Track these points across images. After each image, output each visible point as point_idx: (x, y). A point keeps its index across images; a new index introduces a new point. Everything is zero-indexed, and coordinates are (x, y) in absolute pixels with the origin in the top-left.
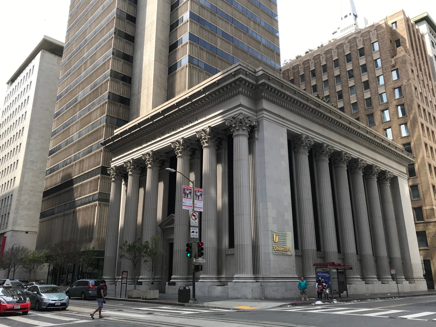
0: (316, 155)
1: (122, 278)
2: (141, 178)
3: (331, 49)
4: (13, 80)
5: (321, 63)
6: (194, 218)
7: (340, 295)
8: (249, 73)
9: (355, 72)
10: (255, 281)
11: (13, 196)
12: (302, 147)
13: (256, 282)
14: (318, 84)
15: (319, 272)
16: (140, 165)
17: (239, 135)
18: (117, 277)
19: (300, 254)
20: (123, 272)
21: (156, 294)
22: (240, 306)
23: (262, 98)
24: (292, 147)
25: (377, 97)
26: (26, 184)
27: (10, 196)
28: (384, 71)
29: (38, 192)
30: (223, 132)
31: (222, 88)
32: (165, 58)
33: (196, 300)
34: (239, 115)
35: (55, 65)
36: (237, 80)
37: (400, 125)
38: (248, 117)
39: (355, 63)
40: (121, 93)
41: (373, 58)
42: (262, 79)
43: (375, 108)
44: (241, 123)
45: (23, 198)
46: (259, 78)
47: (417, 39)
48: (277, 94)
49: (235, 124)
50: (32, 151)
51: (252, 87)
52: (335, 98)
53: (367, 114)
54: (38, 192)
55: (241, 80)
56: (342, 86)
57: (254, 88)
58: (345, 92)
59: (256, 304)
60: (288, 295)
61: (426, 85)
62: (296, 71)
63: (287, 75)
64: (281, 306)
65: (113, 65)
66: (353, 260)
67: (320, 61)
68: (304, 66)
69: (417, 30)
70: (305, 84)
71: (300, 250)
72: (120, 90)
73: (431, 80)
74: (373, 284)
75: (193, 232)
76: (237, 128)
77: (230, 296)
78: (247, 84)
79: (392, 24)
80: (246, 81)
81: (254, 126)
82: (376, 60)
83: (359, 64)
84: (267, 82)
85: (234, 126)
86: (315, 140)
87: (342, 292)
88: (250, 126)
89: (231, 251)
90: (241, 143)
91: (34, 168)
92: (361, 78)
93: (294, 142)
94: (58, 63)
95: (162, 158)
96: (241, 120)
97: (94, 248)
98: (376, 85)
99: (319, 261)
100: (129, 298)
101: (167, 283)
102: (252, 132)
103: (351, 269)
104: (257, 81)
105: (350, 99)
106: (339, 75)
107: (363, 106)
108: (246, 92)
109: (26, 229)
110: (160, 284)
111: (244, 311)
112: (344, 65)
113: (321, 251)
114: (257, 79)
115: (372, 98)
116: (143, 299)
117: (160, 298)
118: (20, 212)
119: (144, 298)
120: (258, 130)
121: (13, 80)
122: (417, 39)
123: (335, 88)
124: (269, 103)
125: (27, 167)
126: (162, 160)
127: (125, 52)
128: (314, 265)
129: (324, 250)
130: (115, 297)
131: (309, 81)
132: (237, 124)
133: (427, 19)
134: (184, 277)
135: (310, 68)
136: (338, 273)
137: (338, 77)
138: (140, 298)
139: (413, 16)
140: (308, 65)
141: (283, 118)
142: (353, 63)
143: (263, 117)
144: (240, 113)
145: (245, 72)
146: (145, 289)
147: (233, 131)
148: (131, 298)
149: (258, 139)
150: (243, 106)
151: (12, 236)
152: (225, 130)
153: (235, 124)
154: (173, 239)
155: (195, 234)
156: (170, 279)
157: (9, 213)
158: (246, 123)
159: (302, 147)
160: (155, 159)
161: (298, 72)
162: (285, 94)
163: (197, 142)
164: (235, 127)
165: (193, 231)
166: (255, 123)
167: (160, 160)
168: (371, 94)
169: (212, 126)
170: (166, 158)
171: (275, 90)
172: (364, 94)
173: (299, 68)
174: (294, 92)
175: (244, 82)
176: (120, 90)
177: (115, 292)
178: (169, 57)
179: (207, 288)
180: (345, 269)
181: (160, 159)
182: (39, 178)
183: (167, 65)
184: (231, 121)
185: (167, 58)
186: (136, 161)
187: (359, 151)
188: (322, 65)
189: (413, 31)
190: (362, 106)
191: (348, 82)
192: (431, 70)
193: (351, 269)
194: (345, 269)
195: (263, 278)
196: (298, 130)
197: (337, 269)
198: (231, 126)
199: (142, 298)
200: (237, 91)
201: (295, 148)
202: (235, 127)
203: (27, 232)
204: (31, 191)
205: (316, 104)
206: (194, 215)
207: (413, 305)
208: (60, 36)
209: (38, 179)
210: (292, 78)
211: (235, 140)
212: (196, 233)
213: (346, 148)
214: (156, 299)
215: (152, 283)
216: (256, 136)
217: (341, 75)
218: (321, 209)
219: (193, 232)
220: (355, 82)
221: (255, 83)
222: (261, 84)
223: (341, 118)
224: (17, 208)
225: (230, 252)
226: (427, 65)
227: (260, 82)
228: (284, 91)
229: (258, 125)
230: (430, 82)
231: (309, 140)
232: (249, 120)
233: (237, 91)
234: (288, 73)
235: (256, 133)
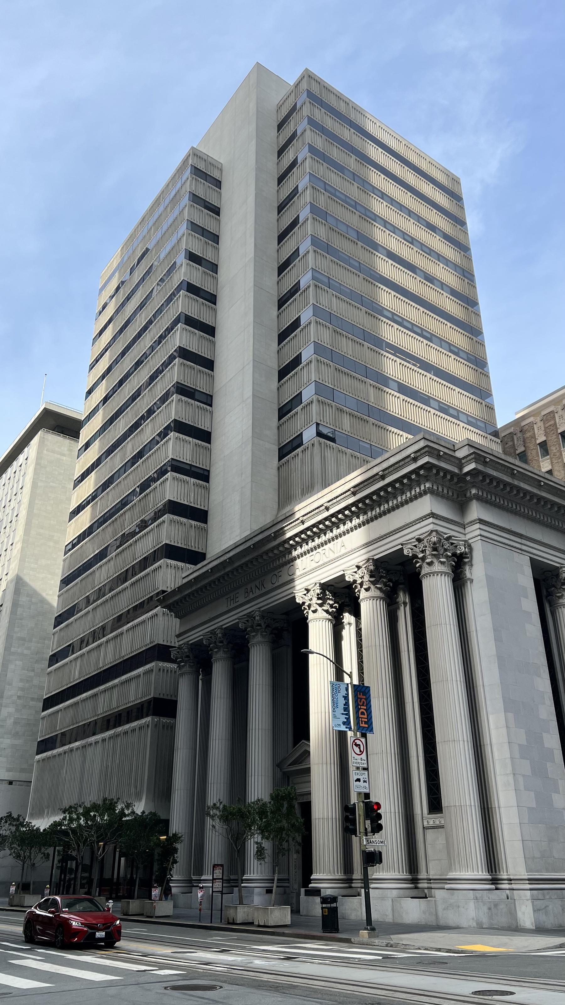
1: (213, 879)
6: (357, 750)
8: (445, 453)
13: (497, 889)
17: (433, 573)
18: (194, 878)
20: (215, 866)
21: (281, 915)
24: (544, 593)
26: (10, 684)
29: (33, 699)
30: (399, 568)
33: (373, 929)
35: (64, 455)
40: (192, 500)
42: (469, 462)
44: (435, 549)
46: (463, 461)
49: (422, 552)
50: (21, 619)
51: (452, 479)
54: (33, 699)
57: (456, 480)
59: (504, 939)
63: (510, 443)
70: (551, 459)
75: (358, 780)
76: (428, 561)
81: (461, 554)
84: (481, 467)
85: (421, 555)
88: (454, 555)
90: (437, 589)
91: (26, 652)
96: (435, 543)
97: (143, 812)
101: (303, 890)
102: (458, 565)
104: (461, 468)
108: (440, 489)
110: (285, 893)
111: (483, 956)
114: (460, 463)
116: (259, 926)
119: (262, 923)
120: (471, 561)
125: (13, 649)
131: (558, 454)
132: (428, 552)
134: (337, 877)
135: (557, 429)
138: (252, 924)
141: (521, 536)
144: (432, 531)
146: (257, 904)
147: (420, 567)
149: (472, 581)
150: (438, 515)
152: (402, 564)
154: (310, 794)
155: (361, 783)
156: (310, 881)
158: (446, 550)
161: (534, 437)
162: (519, 489)
163: (346, 590)
164: (423, 559)
169: (376, 557)
173: (533, 429)
175: (434, 471)
177: (200, 910)
179: (391, 903)
182: (33, 671)
183: (277, 444)
184: (415, 546)
195: (511, 880)
201: (549, 594)
202: (423, 559)
203: (11, 783)
204: (19, 697)
205: (409, 363)
206: (357, 745)
208: (75, 406)
209: (32, 674)
210: (521, 449)
211: (426, 583)
212: (365, 781)
219: (358, 780)
225: (431, 823)
227: (466, 469)
228: (516, 482)
232: (452, 544)
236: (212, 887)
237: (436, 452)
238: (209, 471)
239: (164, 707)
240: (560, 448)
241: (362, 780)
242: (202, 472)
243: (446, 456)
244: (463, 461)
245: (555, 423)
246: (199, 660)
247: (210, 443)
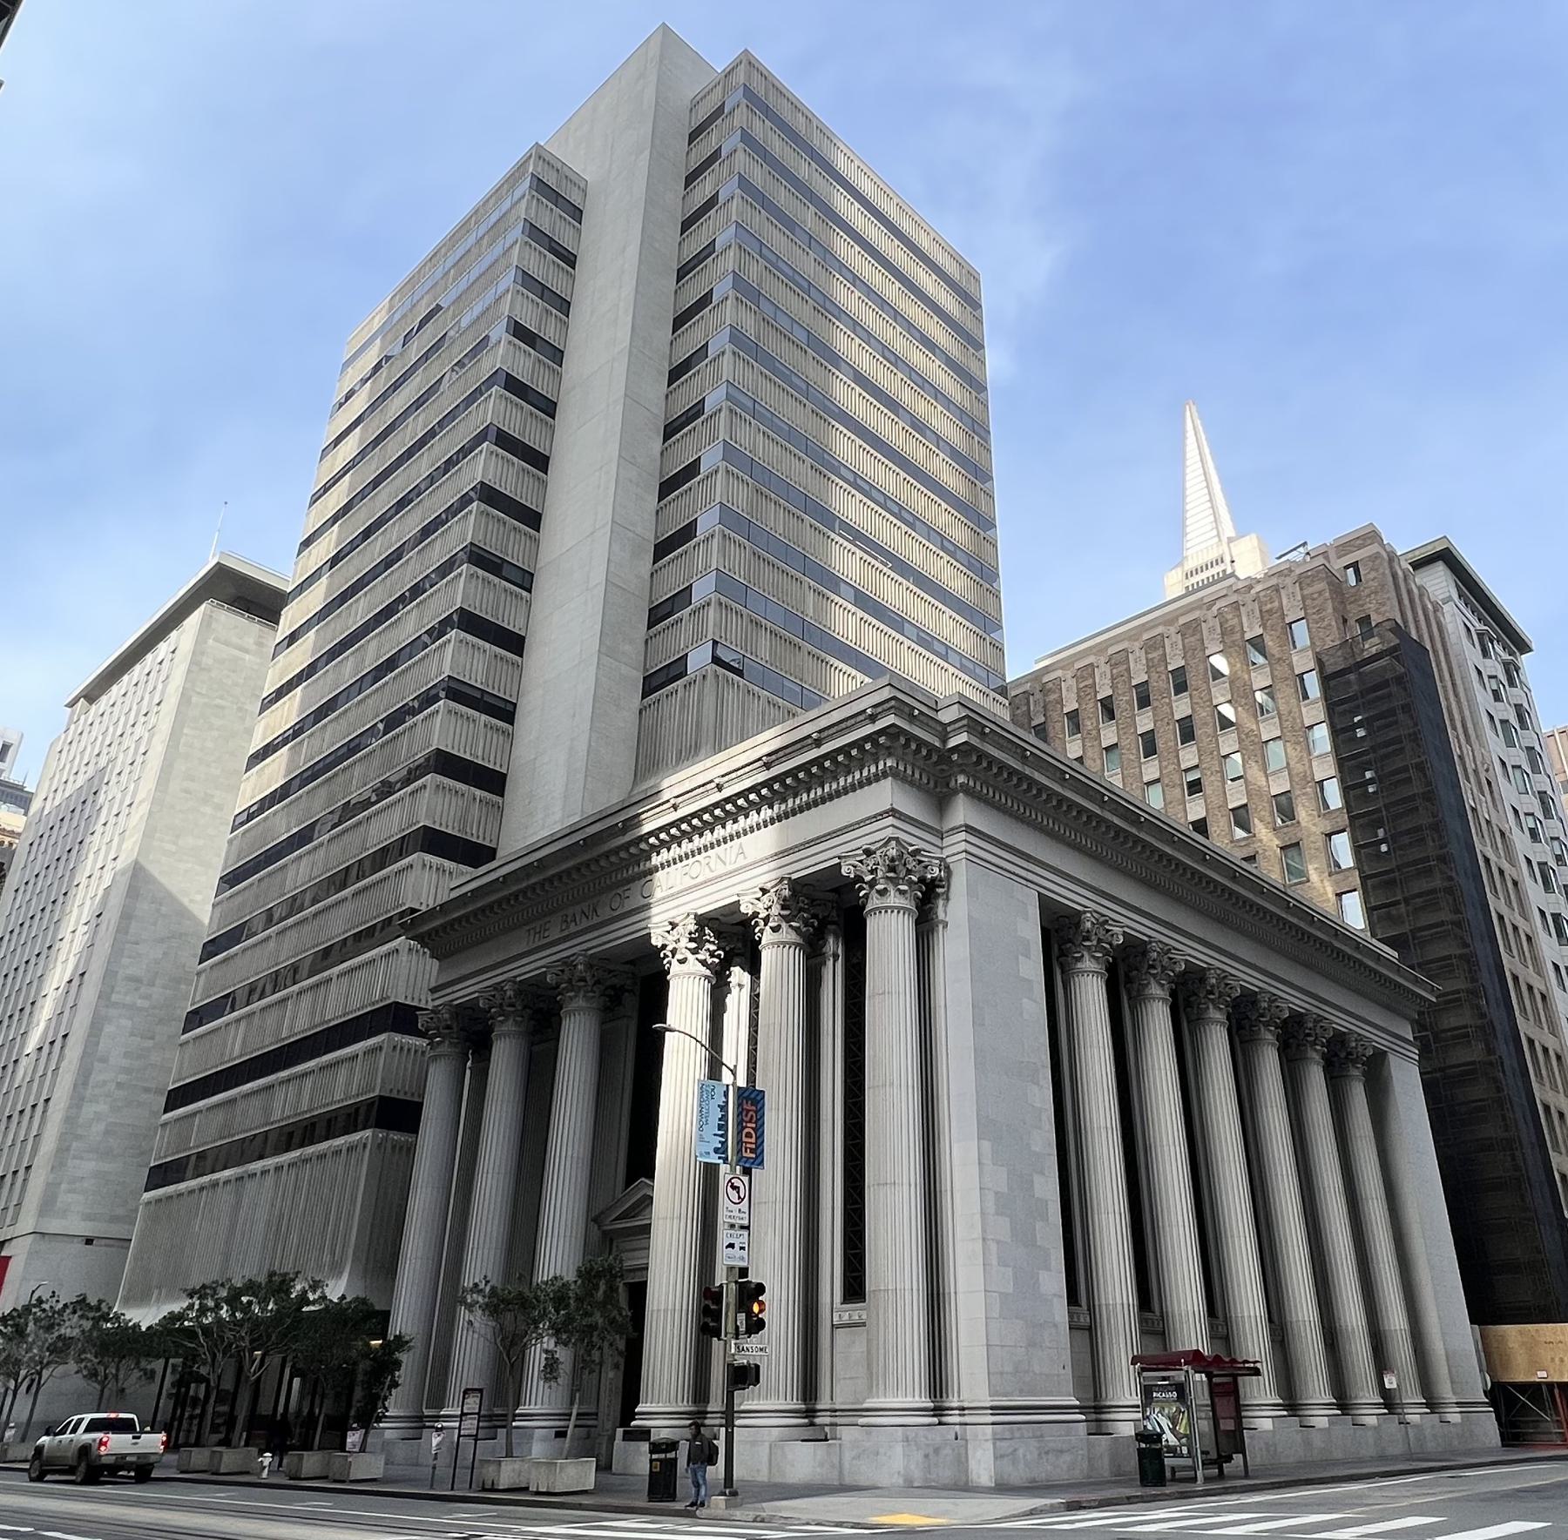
0: (1129, 980)
1: (463, 1414)
2: (536, 1048)
3: (1161, 635)
4: (92, 694)
6: (733, 1195)
10: (936, 1420)
11: (51, 1103)
12: (1087, 956)
13: (940, 1424)
15: (187, 1437)
19: (1084, 1320)
21: (581, 1474)
22: (882, 1513)
26: (104, 1060)
27: (29, 1109)
29: (147, 1090)
33: (734, 1494)
34: (885, 845)
35: (247, 651)
37: (1329, 835)
41: (1292, 669)
42: (958, 731)
44: (892, 869)
45: (88, 1110)
47: (1406, 602)
48: (1017, 785)
49: (872, 872)
54: (147, 1090)
57: (935, 758)
59: (945, 1504)
60: (1044, 1470)
61: (1470, 771)
64: (1032, 1513)
66: (1254, 1343)
67: (1128, 670)
69: (1419, 588)
70: (1083, 740)
71: (1085, 1307)
73: (1468, 741)
75: (731, 1246)
76: (879, 887)
77: (848, 1480)
78: (924, 752)
79: (1347, 567)
80: (910, 738)
81: (933, 879)
82: (1301, 676)
85: (868, 878)
87: (1229, 1459)
88: (922, 880)
89: (853, 1312)
93: (1061, 935)
94: (260, 644)
95: (615, 981)
96: (893, 860)
99: (1154, 1349)
100: (484, 1490)
101: (620, 1431)
102: (927, 899)
103: (1257, 1372)
108: (909, 772)
109: (86, 1229)
110: (588, 1437)
112: (1204, 687)
114: (944, 731)
117: (599, 1489)
118: (70, 1163)
121: (92, 694)
122: (1406, 602)
124: (1008, 820)
125: (114, 998)
126: (613, 987)
128: (1134, 1361)
130: (432, 1487)
132: (880, 874)
133: (1446, 557)
136: (1214, 1390)
139: (1405, 541)
140: (1090, 681)
145: (907, 709)
148: (493, 1490)
149: (946, 925)
151: (32, 1254)
152: (836, 890)
153: (872, 872)
157: (28, 1168)
158: (909, 872)
164: (872, 884)
169: (794, 876)
171: (1003, 766)
180: (1235, 1377)
182: (152, 1038)
188: (1134, 683)
189: (1409, 592)
192: (1467, 713)
193: (1257, 1372)
196: (1071, 897)
197: (1210, 1376)
198: (859, 879)
199: (533, 1488)
202: (872, 884)
203: (89, 1241)
204: (119, 1085)
206: (733, 1187)
207: (1467, 1499)
214: (585, 1492)
215: (561, 1434)
216: (941, 915)
219: (731, 1246)
224: (62, 1150)
225: (846, 1317)
226: (1456, 695)
227: (952, 743)
228: (1028, 771)
230: (1466, 749)
232: (920, 862)
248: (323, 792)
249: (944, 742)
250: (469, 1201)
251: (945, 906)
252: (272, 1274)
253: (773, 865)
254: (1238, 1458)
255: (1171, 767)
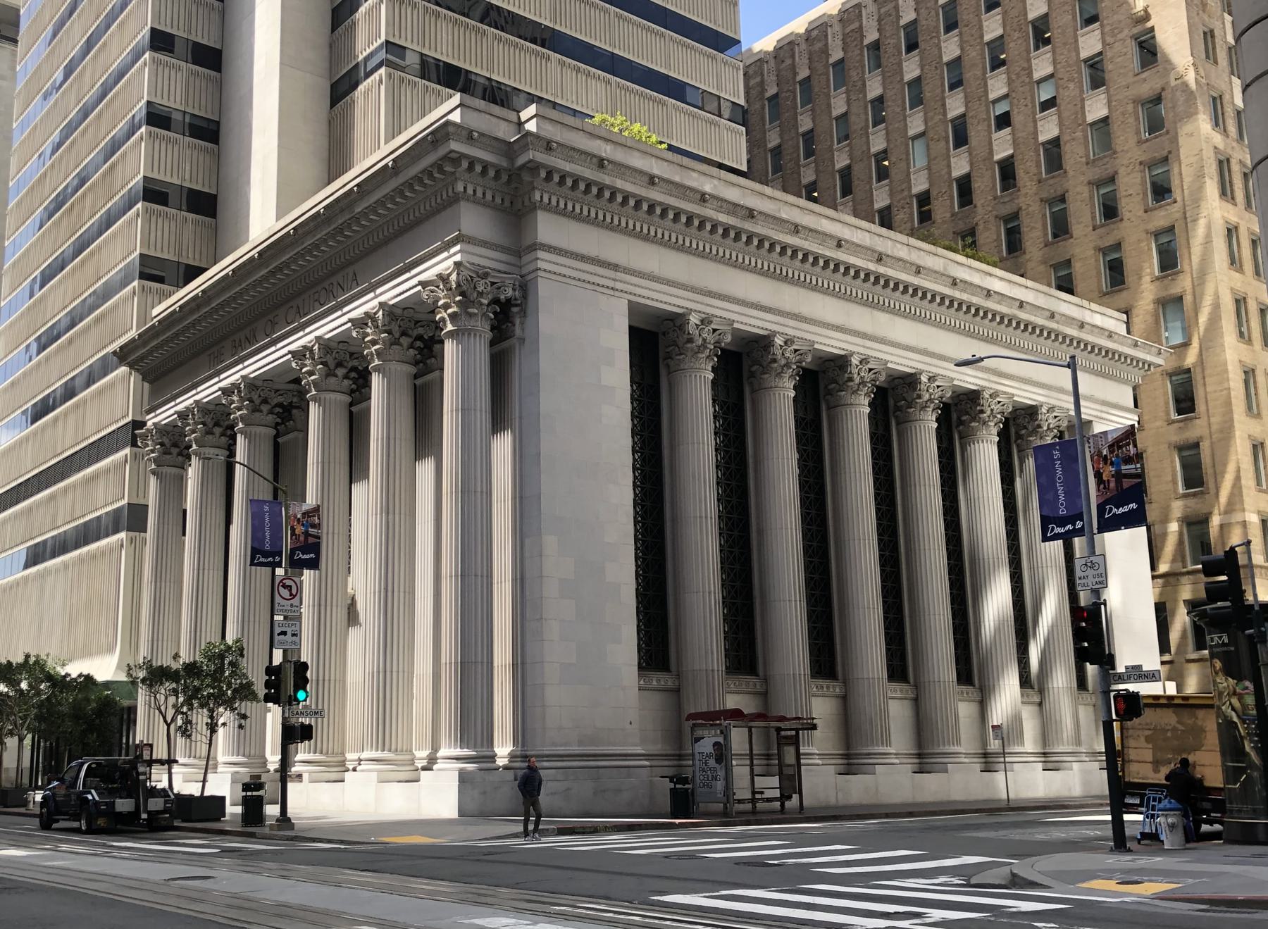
5: (899, 17)
6: (285, 593)
7: (782, 805)
9: (1012, 45)
14: (889, 94)
16: (216, 420)
23: (535, 208)
25: (1079, 134)
28: (1109, 40)
31: (409, 184)
32: (316, 56)
36: (445, 158)
38: (486, 275)
39: (1013, 13)
40: (187, 177)
43: (1071, 173)
52: (943, 143)
53: (1044, 195)
55: (455, 159)
56: (966, 97)
58: (975, 122)
62: (818, 45)
63: (788, 62)
65: (154, 88)
68: (844, 27)
70: (847, 92)
72: (180, 164)
74: (946, 771)
75: (284, 633)
81: (508, 300)
83: (1026, 14)
86: (736, 325)
87: (790, 797)
88: (495, 301)
92: (1030, 67)
95: (281, 399)
98: (1077, 92)
105: (990, 144)
106: (959, 58)
107: (1034, 170)
113: (757, 675)
115: (1064, 138)
123: (944, 105)
126: (280, 405)
127: (192, 38)
129: (765, 671)
135: (862, 37)
137: (997, 45)
140: (856, 25)
142: (1005, 14)
143: (538, 269)
158: (481, 294)
159: (689, 354)
160: (257, 402)
165: (284, 629)
166: (510, 293)
167: (277, 405)
168: (1061, 125)
170: (281, 405)
172: (1039, 124)
173: (826, 36)
174: (646, 179)
176: (180, 164)
178: (331, 46)
181: (275, 401)
185: (327, 51)
186: (211, 407)
187: (922, 345)
190: (986, 186)
191: (986, 85)
193: (814, 727)
194: (797, 730)
200: (450, 193)
206: (285, 586)
213: (869, 344)
216: (518, 332)
217: (966, 60)
218: (761, 544)
219: (284, 633)
220: (1010, 82)
221: (505, 164)
222: (523, 166)
223: (839, 245)
227: (521, 161)
229: (525, 297)
231: (715, 330)
233: (450, 193)
234: (793, 56)
235: (517, 321)
236: (752, 775)
237: (464, 133)
238: (218, 123)
239: (134, 518)
240: (863, 72)
241: (289, 634)
242: (204, 124)
243: (483, 139)
244: (516, 147)
245: (861, 27)
246: (173, 447)
247: (219, 70)
248: (66, 223)
249: (512, 159)
250: (748, 560)
251: (522, 323)
252: (27, 656)
253: (503, 257)
254: (795, 797)
255: (937, 118)
